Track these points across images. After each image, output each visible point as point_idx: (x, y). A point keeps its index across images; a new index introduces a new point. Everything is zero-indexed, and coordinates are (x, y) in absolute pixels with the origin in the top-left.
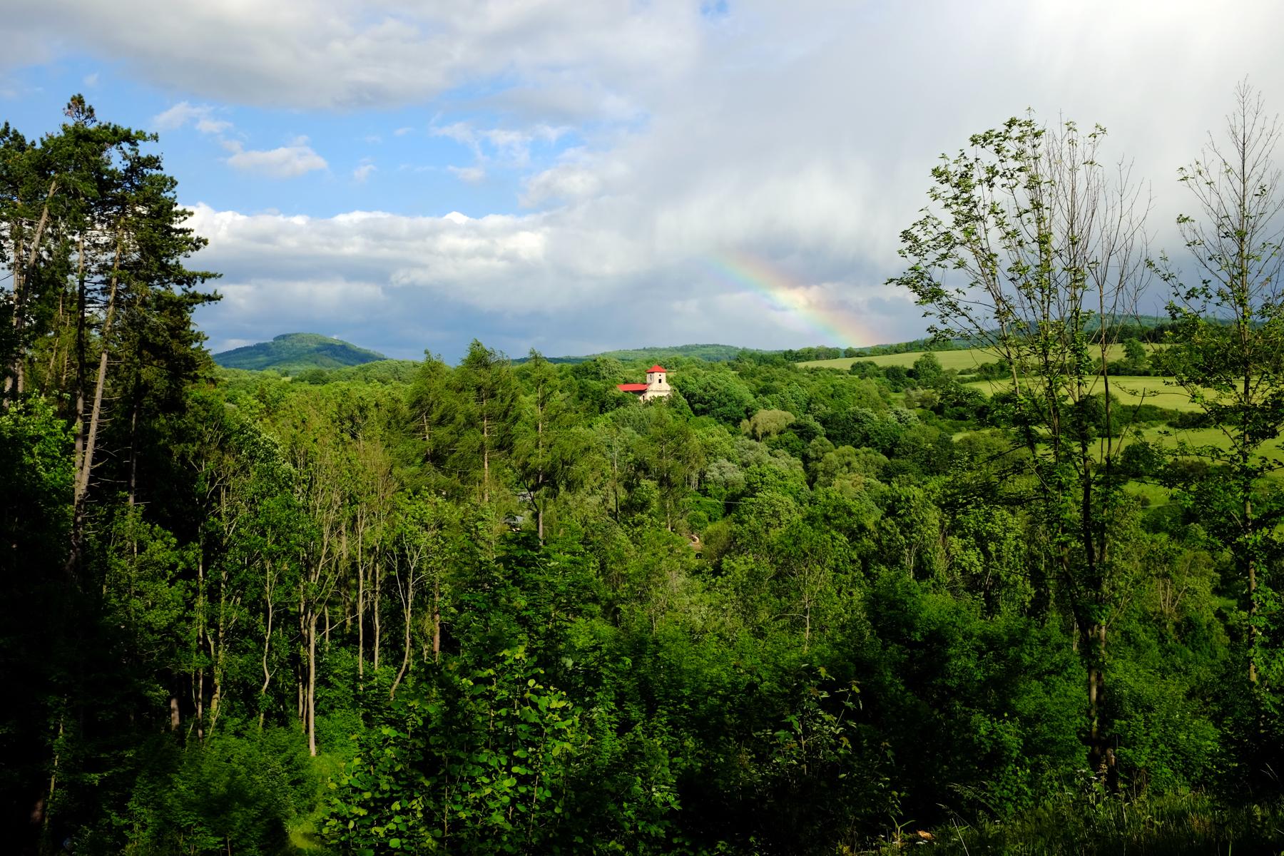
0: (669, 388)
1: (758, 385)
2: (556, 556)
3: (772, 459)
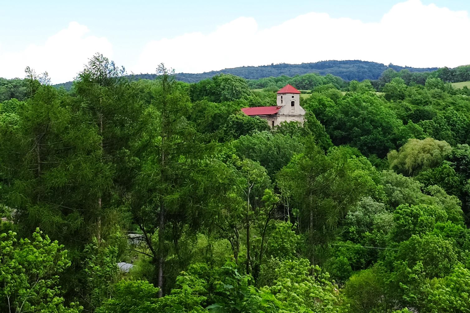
0: (303, 112)
1: (407, 109)
2: (189, 279)
3: (426, 197)
